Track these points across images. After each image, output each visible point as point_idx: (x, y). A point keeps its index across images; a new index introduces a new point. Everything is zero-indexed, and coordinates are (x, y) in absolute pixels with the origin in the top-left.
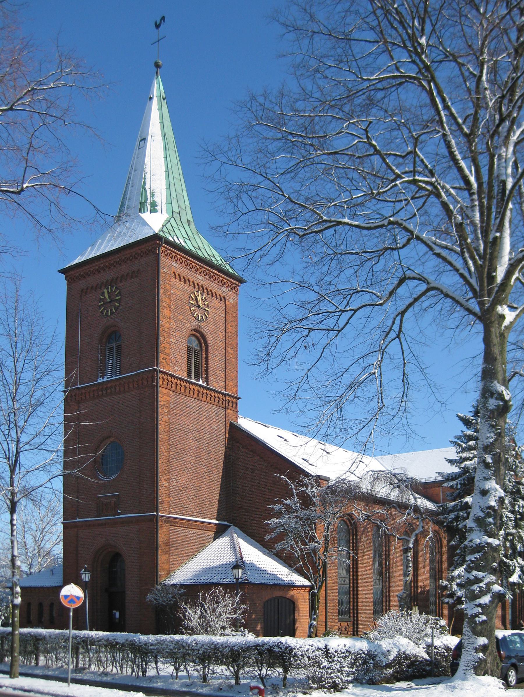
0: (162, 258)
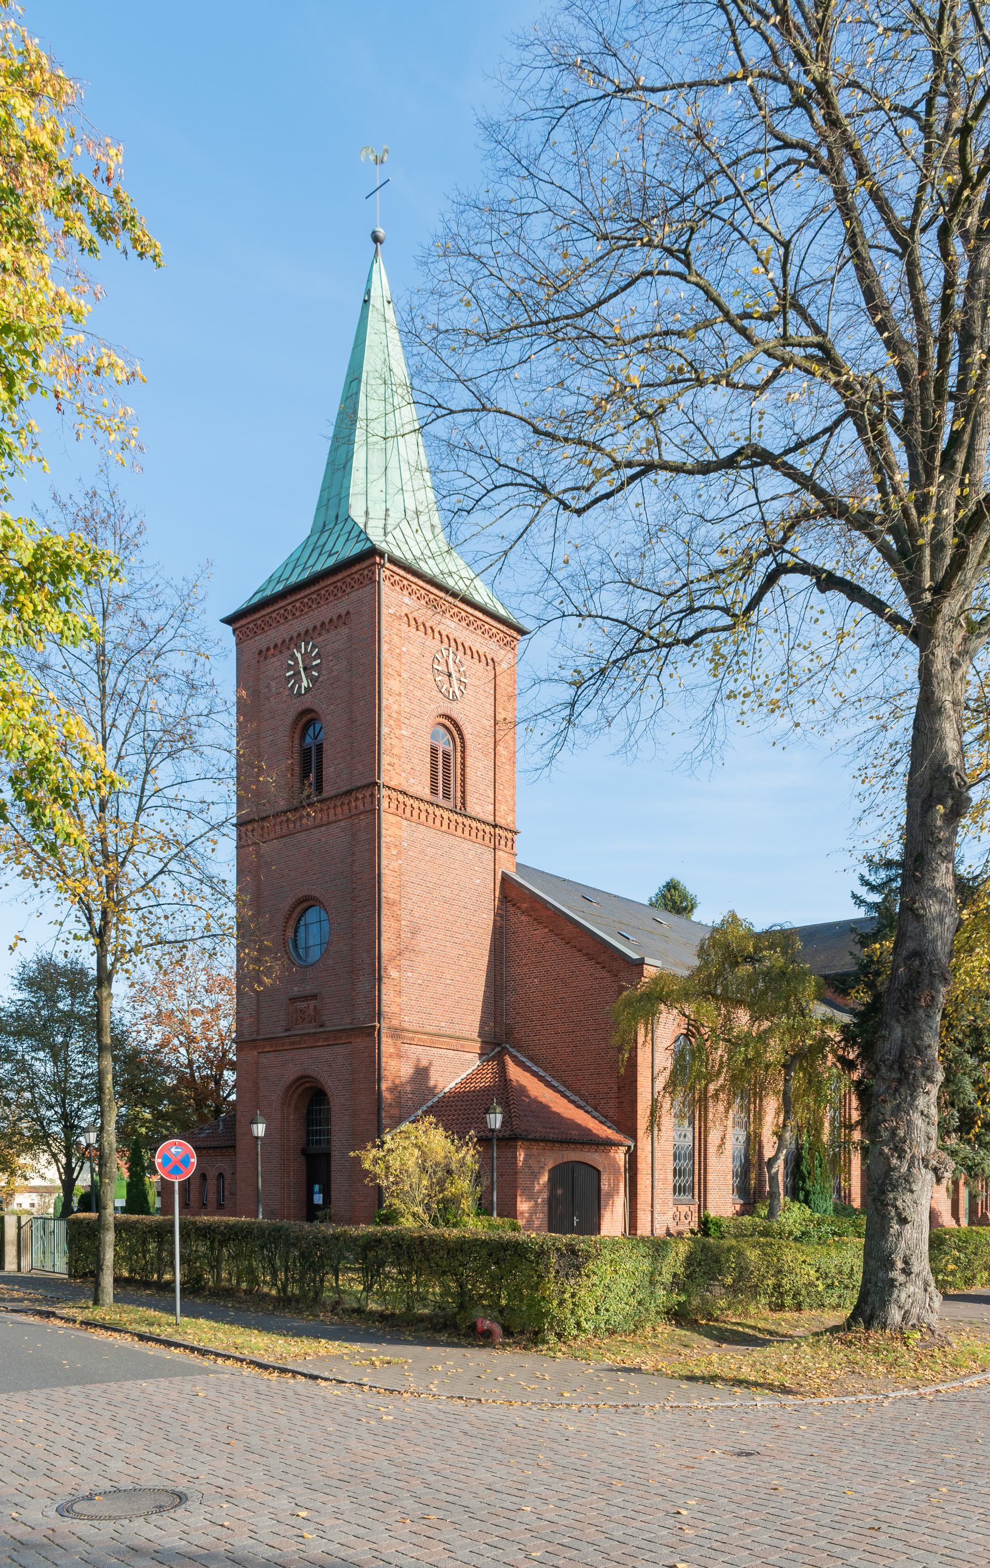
0: (385, 587)
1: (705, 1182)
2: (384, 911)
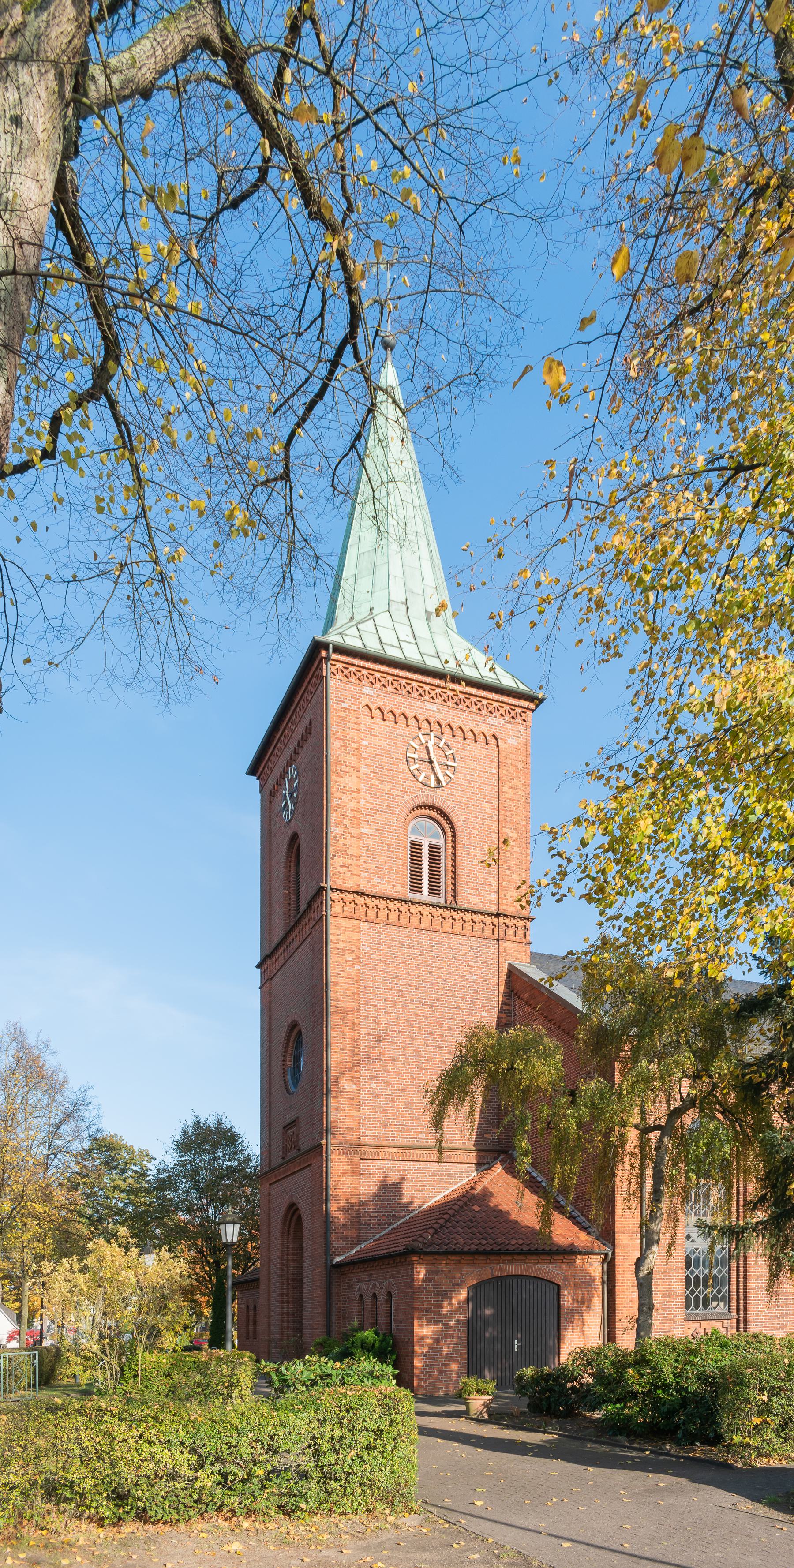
1: (745, 1292)
2: (333, 1020)
